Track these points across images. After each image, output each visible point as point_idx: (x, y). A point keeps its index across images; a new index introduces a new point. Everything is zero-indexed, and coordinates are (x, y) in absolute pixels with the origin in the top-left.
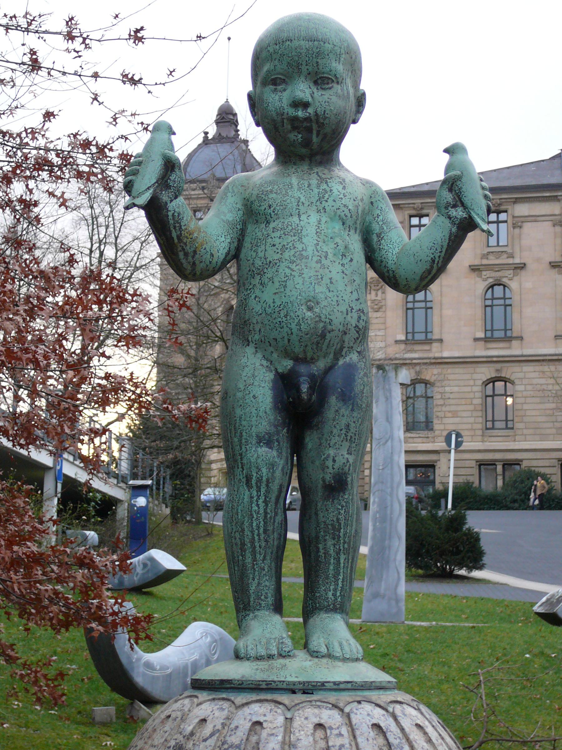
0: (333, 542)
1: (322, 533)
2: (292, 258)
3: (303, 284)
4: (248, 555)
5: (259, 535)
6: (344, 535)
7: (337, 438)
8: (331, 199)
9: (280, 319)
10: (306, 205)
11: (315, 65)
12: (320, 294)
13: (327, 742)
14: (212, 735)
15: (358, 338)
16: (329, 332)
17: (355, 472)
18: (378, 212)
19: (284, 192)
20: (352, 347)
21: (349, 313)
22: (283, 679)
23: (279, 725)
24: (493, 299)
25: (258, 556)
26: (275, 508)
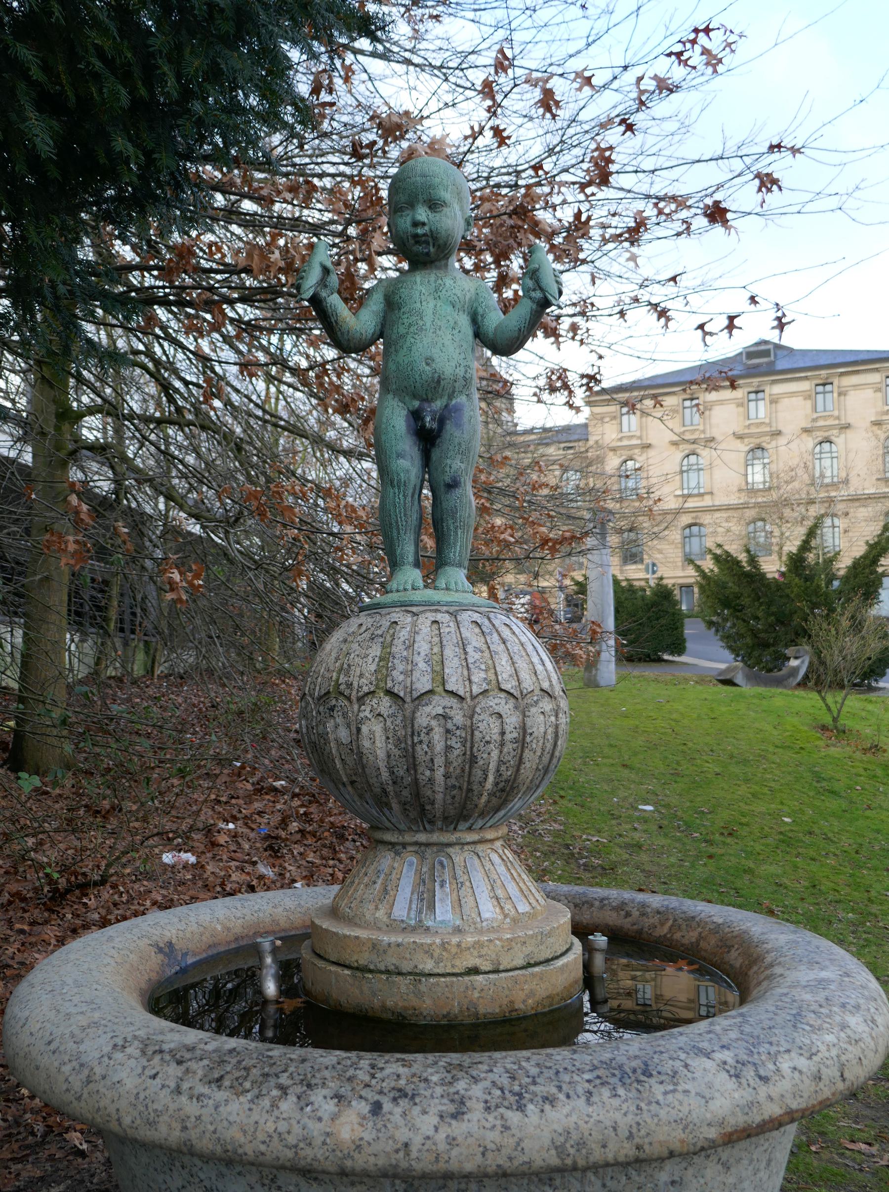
4: (395, 531)
24: (821, 453)
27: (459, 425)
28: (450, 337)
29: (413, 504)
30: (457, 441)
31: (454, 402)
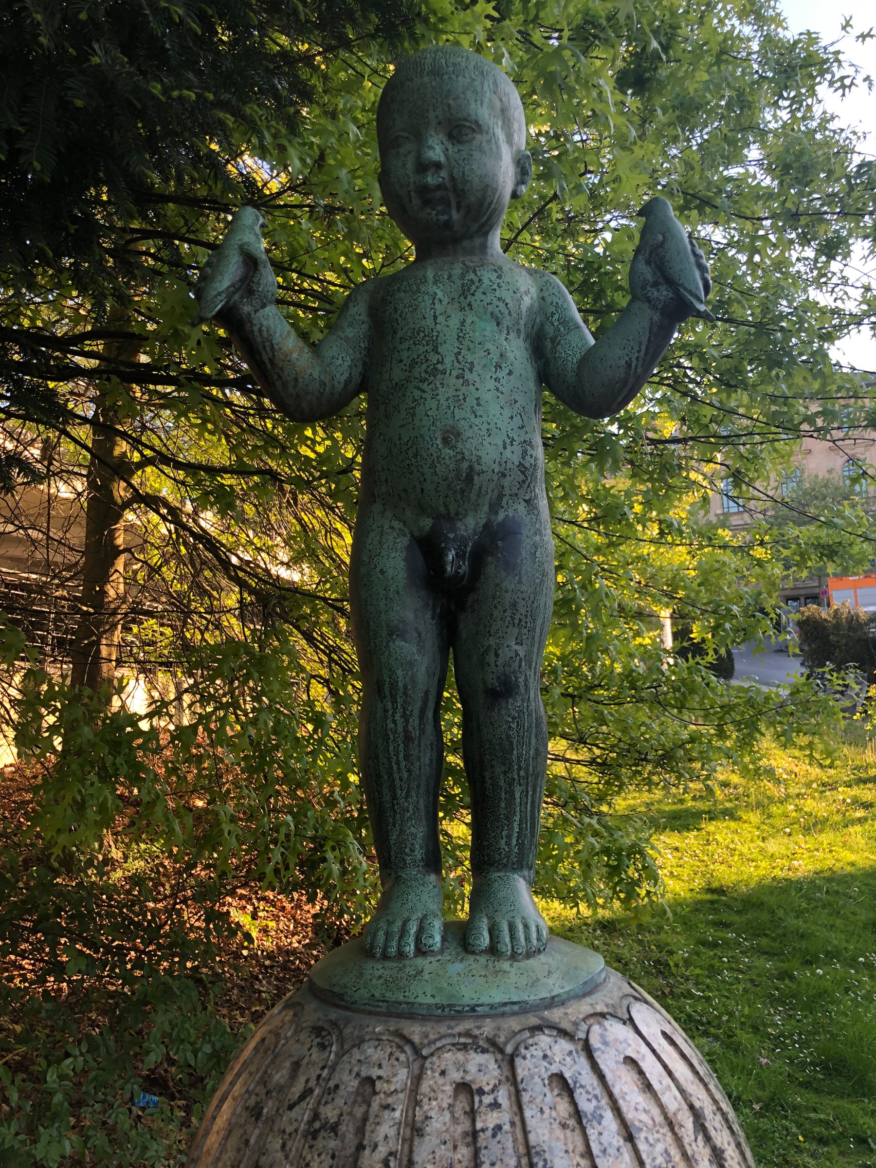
0: (503, 768)
1: (487, 756)
2: (423, 375)
3: (438, 409)
4: (386, 791)
5: (398, 763)
6: (518, 758)
7: (499, 622)
8: (481, 290)
9: (408, 462)
10: (445, 302)
11: (446, 109)
12: (462, 422)
13: (474, 1122)
14: (302, 1097)
15: (524, 482)
16: (478, 474)
17: (530, 668)
18: (553, 309)
19: (415, 288)
20: (516, 495)
21: (508, 447)
22: (411, 1000)
23: (399, 1086)
25: (399, 791)
26: (420, 724)
27: (510, 566)
28: (491, 384)
29: (422, 731)
30: (508, 598)
31: (501, 516)
